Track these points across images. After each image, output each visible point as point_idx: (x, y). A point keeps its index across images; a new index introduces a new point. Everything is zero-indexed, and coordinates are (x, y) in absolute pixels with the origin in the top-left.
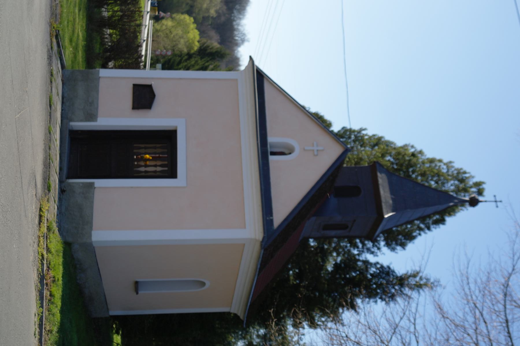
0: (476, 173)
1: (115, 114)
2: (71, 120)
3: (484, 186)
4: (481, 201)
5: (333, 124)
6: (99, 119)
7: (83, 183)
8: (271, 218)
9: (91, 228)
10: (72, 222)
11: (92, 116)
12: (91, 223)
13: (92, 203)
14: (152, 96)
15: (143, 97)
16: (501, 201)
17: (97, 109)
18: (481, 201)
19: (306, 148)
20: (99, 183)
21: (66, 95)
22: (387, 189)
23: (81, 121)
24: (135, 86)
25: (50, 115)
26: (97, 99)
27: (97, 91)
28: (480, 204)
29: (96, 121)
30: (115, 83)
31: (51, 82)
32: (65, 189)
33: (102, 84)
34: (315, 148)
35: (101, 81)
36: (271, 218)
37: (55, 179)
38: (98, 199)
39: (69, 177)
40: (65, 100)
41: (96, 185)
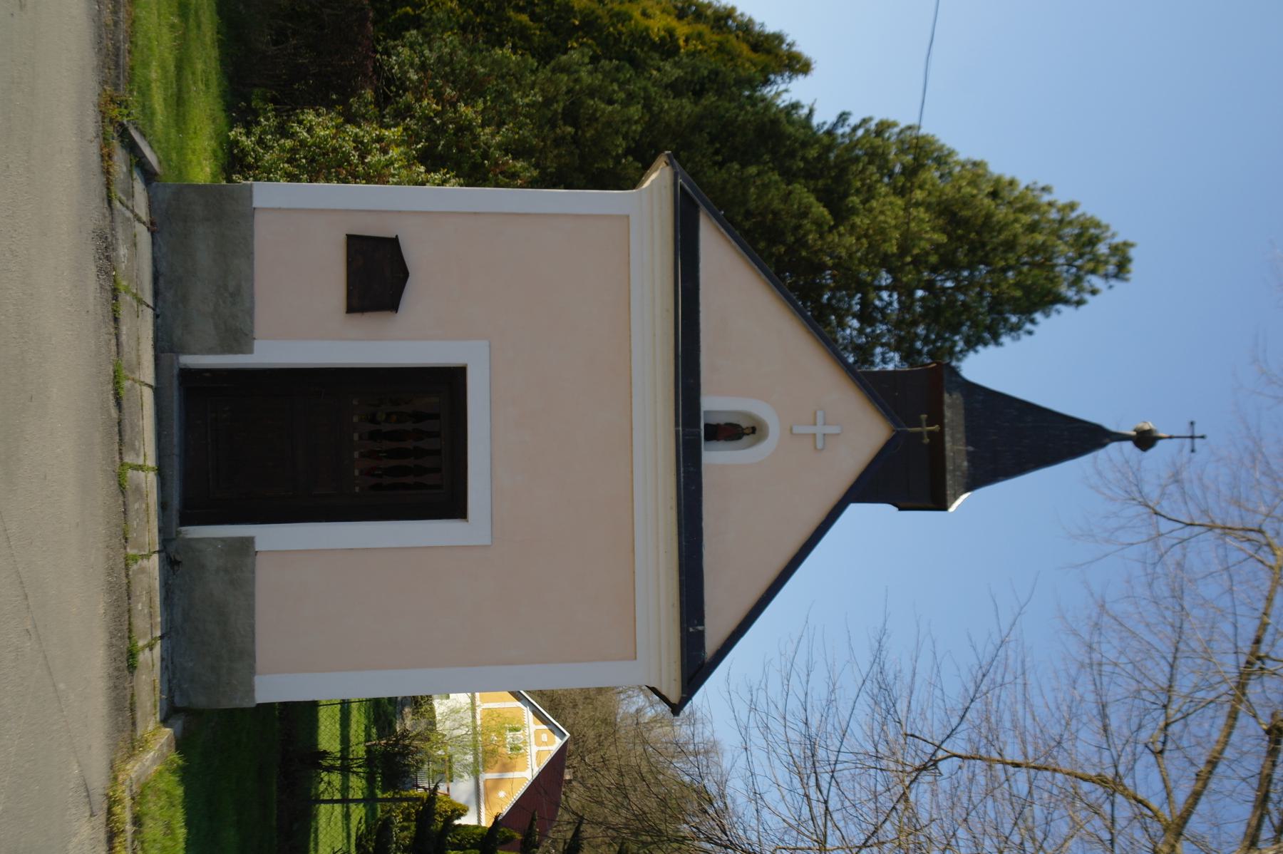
0: (1119, 224)
1: (301, 329)
2: (184, 350)
3: (1132, 253)
4: (1161, 438)
5: (809, 77)
6: (257, 344)
7: (223, 540)
8: (700, 628)
9: (252, 671)
10: (199, 625)
11: (239, 339)
12: (252, 656)
13: (251, 596)
14: (401, 274)
15: (376, 275)
16: (1202, 437)
17: (250, 313)
18: (1161, 438)
19: (797, 430)
20: (270, 537)
21: (163, 267)
22: (960, 435)
23: (211, 351)
24: (352, 239)
25: (121, 434)
26: (250, 279)
27: (250, 256)
28: (1160, 443)
29: (251, 352)
30: (300, 221)
31: (116, 320)
32: (178, 558)
33: (264, 235)
34: (820, 430)
35: (259, 218)
36: (700, 628)
37: (149, 534)
38: (268, 584)
39: (187, 520)
40: (161, 280)
41: (259, 546)
